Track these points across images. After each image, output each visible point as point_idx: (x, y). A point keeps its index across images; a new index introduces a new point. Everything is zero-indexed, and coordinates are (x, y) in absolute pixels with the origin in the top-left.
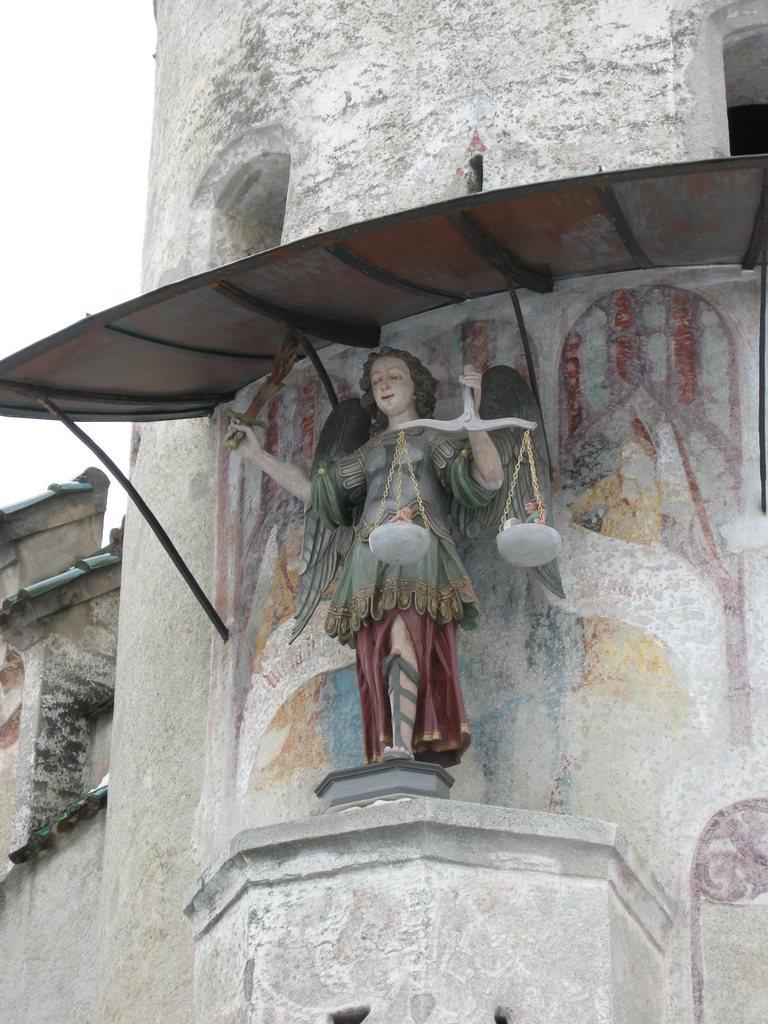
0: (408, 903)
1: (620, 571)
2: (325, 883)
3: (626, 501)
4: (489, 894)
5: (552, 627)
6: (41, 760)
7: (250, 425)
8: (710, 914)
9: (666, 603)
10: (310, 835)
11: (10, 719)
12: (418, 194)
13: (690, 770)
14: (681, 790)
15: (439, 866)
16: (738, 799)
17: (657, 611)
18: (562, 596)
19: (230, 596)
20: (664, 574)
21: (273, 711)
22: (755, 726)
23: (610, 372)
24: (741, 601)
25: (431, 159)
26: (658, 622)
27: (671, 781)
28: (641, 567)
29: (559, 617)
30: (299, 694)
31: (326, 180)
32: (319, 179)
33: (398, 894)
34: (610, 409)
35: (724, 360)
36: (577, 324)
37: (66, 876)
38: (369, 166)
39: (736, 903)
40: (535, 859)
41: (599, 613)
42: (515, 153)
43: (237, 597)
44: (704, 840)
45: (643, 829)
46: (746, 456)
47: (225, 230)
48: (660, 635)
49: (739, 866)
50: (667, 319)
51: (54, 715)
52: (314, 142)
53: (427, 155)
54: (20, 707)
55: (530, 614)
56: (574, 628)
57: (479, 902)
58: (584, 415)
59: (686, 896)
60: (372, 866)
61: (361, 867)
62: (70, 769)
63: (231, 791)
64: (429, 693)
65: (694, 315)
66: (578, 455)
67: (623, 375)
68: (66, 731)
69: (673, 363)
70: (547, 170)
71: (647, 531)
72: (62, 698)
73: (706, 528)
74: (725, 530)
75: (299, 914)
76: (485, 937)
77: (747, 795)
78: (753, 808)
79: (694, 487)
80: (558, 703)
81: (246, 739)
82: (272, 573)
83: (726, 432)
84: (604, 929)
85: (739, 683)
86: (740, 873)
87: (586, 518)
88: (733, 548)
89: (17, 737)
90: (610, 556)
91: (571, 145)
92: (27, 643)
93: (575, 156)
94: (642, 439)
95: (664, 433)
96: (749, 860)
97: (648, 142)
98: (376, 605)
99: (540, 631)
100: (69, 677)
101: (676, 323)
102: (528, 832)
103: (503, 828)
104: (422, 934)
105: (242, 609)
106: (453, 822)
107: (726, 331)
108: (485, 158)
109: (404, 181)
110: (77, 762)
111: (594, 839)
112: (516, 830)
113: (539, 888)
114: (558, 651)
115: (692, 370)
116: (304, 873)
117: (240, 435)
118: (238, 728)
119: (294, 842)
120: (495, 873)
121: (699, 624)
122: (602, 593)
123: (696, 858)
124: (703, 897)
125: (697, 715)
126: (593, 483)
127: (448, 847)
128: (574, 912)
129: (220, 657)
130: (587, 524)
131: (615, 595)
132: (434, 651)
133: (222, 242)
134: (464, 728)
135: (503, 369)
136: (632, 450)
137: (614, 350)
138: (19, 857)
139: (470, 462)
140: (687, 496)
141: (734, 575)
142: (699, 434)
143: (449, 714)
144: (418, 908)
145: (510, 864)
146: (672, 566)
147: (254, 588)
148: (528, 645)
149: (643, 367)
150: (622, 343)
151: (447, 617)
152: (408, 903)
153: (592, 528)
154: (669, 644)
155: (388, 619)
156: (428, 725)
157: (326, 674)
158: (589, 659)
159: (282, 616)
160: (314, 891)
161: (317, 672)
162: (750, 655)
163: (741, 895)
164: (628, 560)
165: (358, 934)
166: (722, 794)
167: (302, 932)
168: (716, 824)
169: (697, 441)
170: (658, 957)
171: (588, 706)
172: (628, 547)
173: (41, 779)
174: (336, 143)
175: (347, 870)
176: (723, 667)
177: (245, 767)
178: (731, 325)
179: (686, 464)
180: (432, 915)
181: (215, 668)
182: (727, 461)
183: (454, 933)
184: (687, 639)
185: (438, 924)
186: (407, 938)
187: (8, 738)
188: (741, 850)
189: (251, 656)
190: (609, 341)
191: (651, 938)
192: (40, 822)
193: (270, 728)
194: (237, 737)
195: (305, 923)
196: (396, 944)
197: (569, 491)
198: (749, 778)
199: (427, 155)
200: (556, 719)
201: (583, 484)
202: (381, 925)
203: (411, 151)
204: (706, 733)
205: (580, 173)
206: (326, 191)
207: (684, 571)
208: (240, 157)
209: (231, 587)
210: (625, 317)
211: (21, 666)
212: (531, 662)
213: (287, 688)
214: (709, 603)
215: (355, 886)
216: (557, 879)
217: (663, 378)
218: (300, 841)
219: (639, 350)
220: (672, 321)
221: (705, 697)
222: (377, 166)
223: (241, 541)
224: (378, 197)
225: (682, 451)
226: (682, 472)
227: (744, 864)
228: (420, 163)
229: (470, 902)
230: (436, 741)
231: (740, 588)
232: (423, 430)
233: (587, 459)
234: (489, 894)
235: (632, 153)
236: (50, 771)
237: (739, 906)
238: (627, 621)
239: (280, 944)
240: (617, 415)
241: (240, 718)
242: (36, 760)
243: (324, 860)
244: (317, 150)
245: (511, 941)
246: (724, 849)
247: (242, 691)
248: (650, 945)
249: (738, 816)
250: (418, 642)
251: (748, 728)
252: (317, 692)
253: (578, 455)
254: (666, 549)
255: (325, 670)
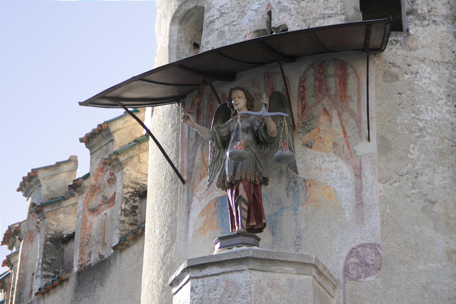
0: (244, 285)
1: (319, 163)
2: (216, 278)
3: (320, 137)
4: (271, 281)
5: (295, 183)
6: (123, 213)
7: (190, 113)
8: (350, 284)
9: (334, 174)
10: (211, 261)
11: (112, 197)
12: (249, 25)
13: (342, 233)
14: (339, 240)
15: (254, 272)
16: (360, 244)
17: (331, 177)
18: (298, 174)
19: (185, 168)
20: (334, 163)
21: (200, 210)
22: (365, 217)
23: (315, 91)
24: (361, 173)
25: (253, 11)
26: (332, 181)
27: (336, 237)
28: (326, 161)
29: (297, 179)
30: (209, 204)
31: (217, 18)
32: (215, 17)
33: (241, 282)
34: (316, 104)
35: (356, 86)
36: (304, 73)
37: (132, 255)
38: (232, 13)
39: (359, 280)
40: (287, 269)
41: (311, 177)
42: (284, 9)
43: (188, 169)
44: (348, 258)
45: (326, 254)
46: (363, 121)
47: (182, 33)
48: (332, 185)
49: (360, 267)
50: (336, 72)
51: (127, 196)
52: (213, 4)
53: (252, 10)
54: (115, 193)
55: (288, 178)
56: (302, 183)
57: (268, 284)
58: (306, 107)
59: (341, 278)
60: (231, 272)
61: (228, 272)
62: (134, 216)
63: (186, 238)
64: (252, 209)
65: (345, 69)
66: (304, 121)
67: (320, 92)
68: (132, 202)
69: (338, 87)
70: (294, 16)
71: (328, 148)
72: (130, 190)
73: (348, 147)
74: (355, 148)
75: (207, 288)
76: (270, 297)
77: (362, 242)
78: (364, 246)
79: (344, 132)
80: (297, 210)
81: (191, 220)
82: (199, 161)
83: (356, 112)
84: (311, 293)
85: (360, 202)
86: (360, 270)
87: (306, 144)
88: (358, 154)
89: (114, 203)
90: (315, 157)
91: (303, 7)
92: (117, 170)
93: (304, 11)
94: (327, 115)
95: (334, 113)
96: (363, 265)
97: (330, 5)
98: (233, 178)
99: (291, 184)
100: (132, 182)
101: (339, 72)
102: (284, 260)
103: (276, 259)
104: (248, 296)
105: (190, 174)
106: (259, 257)
107: (357, 76)
108: (272, 12)
109: (244, 20)
110: (136, 213)
111: (307, 261)
112: (280, 259)
113: (289, 279)
114: (297, 191)
115: (344, 90)
116: (209, 274)
117: (186, 117)
118: (188, 216)
119: (205, 264)
120: (273, 274)
121: (346, 181)
122: (312, 170)
123: (345, 264)
124: (347, 278)
125: (345, 214)
126: (309, 131)
127: (257, 265)
128: (301, 287)
129: (182, 190)
130: (307, 146)
131: (317, 171)
132: (254, 194)
133: (181, 38)
134: (264, 221)
135: (278, 93)
136: (323, 119)
137: (317, 82)
138: (115, 248)
139: (265, 128)
140: (342, 135)
141: (358, 164)
142: (347, 113)
143: (259, 216)
144: (247, 287)
145: (279, 271)
146: (336, 161)
147: (193, 166)
148: (287, 189)
149: (327, 89)
150: (320, 80)
151: (258, 183)
152: (244, 285)
153: (309, 147)
154: (335, 189)
155: (237, 183)
156: (251, 219)
157: (218, 198)
158: (308, 194)
159: (203, 176)
160: (212, 280)
161: (215, 197)
162: (364, 192)
163: (360, 277)
164: (321, 159)
165: (227, 296)
166: (354, 242)
167: (208, 295)
168: (351, 252)
169: (346, 115)
170: (331, 299)
171: (307, 211)
172: (321, 154)
173: (123, 219)
174: (220, 4)
175: (223, 273)
176: (354, 197)
177: (191, 229)
178: (358, 73)
179: (342, 124)
180: (252, 289)
181: (180, 194)
182: (356, 123)
183: (260, 295)
184: (342, 187)
185: (254, 292)
186: (244, 297)
187: (111, 204)
188: (360, 261)
189: (193, 191)
190: (315, 80)
191: (329, 293)
192: (123, 235)
193: (199, 216)
194: (188, 219)
195: (209, 291)
196: (240, 299)
197: (301, 134)
198: (363, 236)
199: (252, 10)
200: (296, 215)
201: (306, 131)
202: (235, 293)
203: (247, 8)
204: (348, 220)
205: (302, 29)
206: (217, 22)
207: (341, 163)
208: (187, 7)
209: (186, 165)
210: (321, 71)
211: (115, 177)
212: (288, 195)
213: (205, 202)
214: (349, 174)
215: (226, 279)
216: (295, 275)
217: (334, 93)
218: (207, 263)
219: (326, 83)
220: (337, 72)
221: (348, 207)
222: (235, 14)
223: (189, 149)
224: (235, 25)
225: (340, 119)
226: (341, 127)
227: (361, 267)
228: (250, 13)
229: (265, 284)
230: (255, 225)
231: (360, 168)
232: (249, 115)
233: (307, 123)
234: (271, 281)
235: (324, 10)
236: (126, 217)
237: (360, 281)
238: (321, 180)
239: (201, 299)
240: (318, 107)
241: (189, 212)
242: (121, 213)
243: (216, 270)
244: (213, 7)
245: (279, 298)
246: (354, 261)
247: (189, 202)
248: (328, 296)
249: (359, 250)
250: (248, 192)
251: (363, 218)
252: (215, 204)
253: (304, 121)
254: (334, 155)
255: (218, 196)
